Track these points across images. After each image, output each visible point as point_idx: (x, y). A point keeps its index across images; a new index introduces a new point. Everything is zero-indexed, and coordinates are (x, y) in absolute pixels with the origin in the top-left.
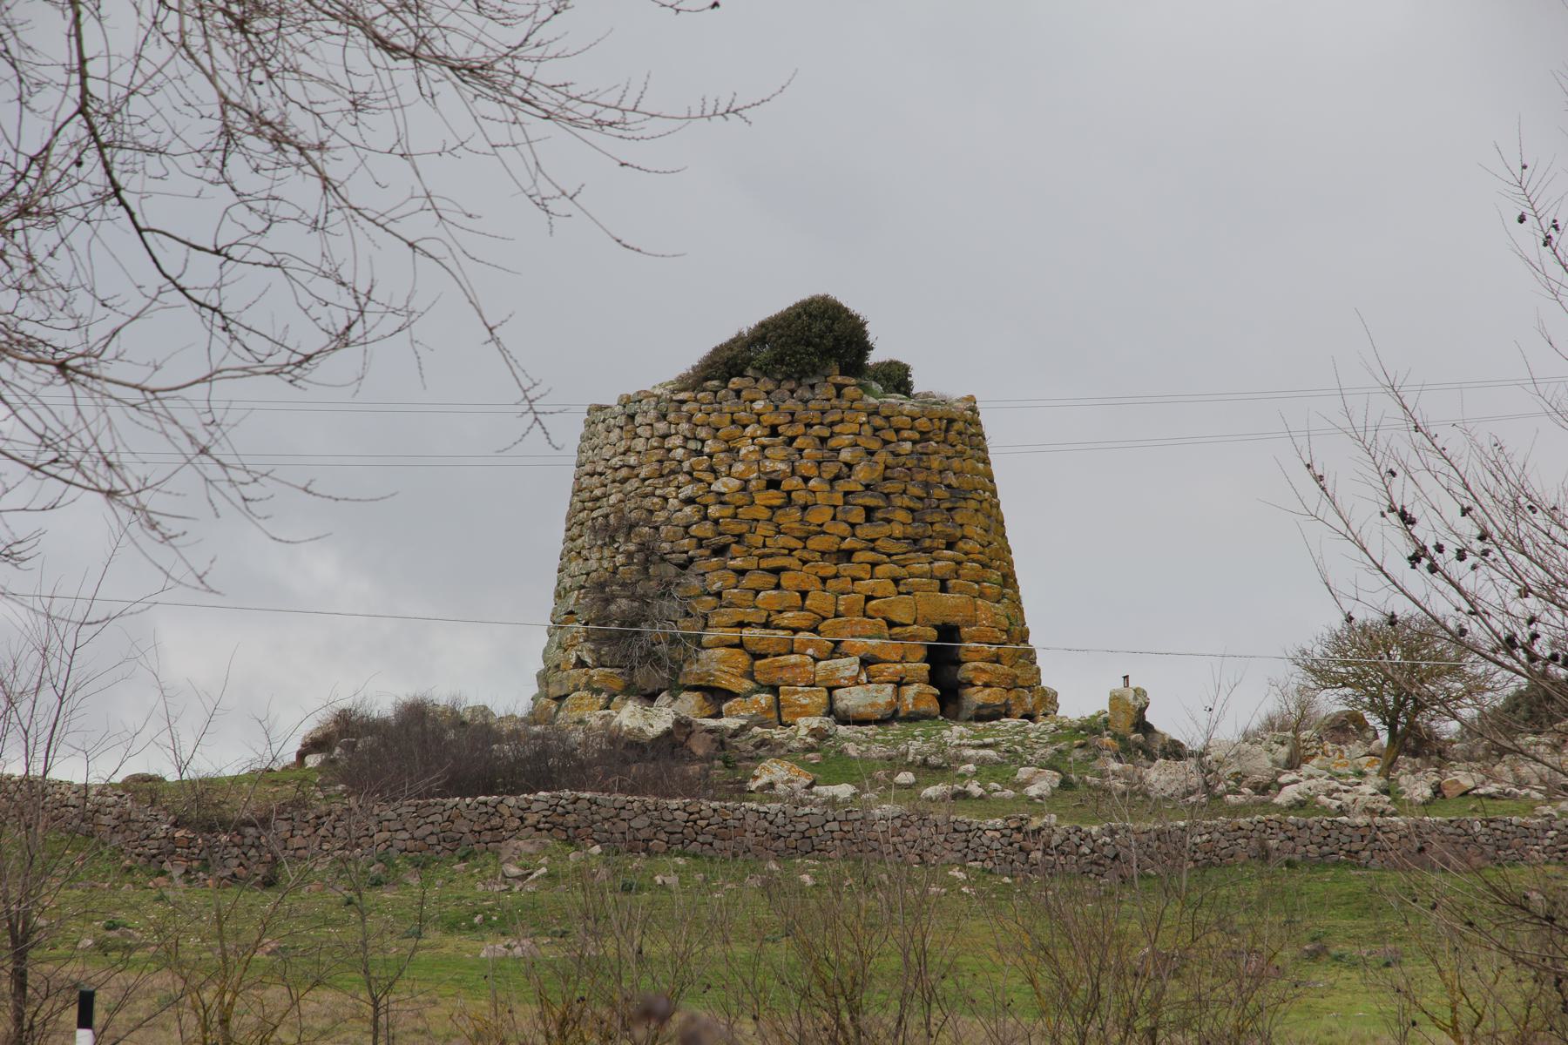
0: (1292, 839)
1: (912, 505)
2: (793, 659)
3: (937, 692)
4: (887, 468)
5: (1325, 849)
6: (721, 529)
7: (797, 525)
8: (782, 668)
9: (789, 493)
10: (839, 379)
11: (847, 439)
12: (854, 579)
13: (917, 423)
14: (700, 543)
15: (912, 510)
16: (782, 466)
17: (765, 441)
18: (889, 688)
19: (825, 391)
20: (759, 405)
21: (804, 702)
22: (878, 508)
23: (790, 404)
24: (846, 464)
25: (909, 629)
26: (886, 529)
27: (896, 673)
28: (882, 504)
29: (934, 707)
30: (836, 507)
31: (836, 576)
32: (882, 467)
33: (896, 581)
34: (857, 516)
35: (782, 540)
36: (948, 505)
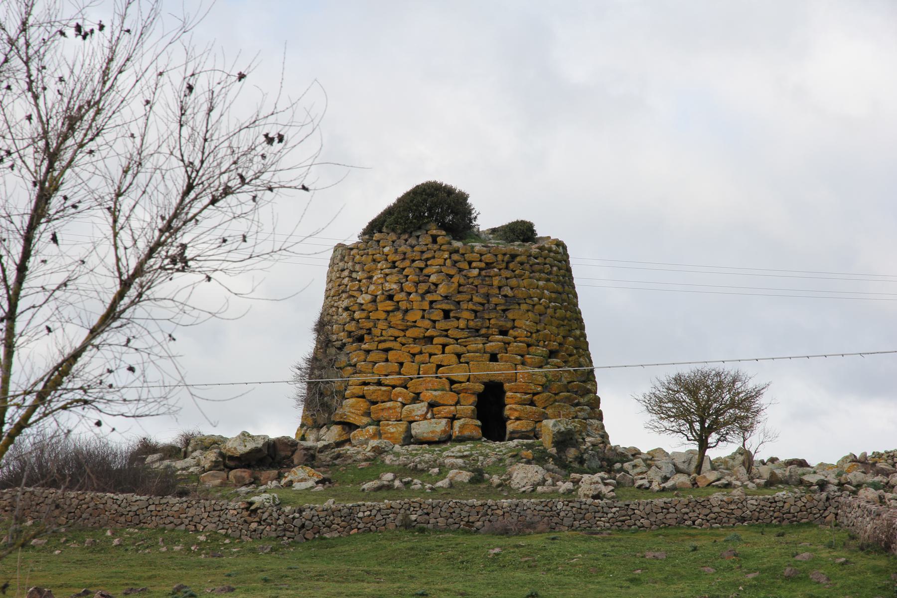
0: (428, 514)
1: (474, 308)
2: (389, 404)
3: (479, 423)
4: (460, 285)
5: (451, 520)
6: (360, 325)
7: (399, 322)
8: (383, 409)
9: (398, 302)
10: (434, 232)
11: (434, 269)
12: (431, 355)
13: (483, 258)
14: (350, 334)
15: (475, 312)
16: (394, 286)
17: (387, 271)
18: (444, 422)
19: (425, 239)
20: (386, 250)
21: (392, 430)
22: (452, 310)
23: (403, 248)
24: (434, 284)
25: (463, 385)
26: (455, 323)
27: (450, 412)
28: (452, 307)
29: (478, 433)
30: (424, 310)
31: (421, 353)
32: (456, 284)
33: (459, 356)
34: (437, 315)
35: (391, 332)
36: (503, 307)
